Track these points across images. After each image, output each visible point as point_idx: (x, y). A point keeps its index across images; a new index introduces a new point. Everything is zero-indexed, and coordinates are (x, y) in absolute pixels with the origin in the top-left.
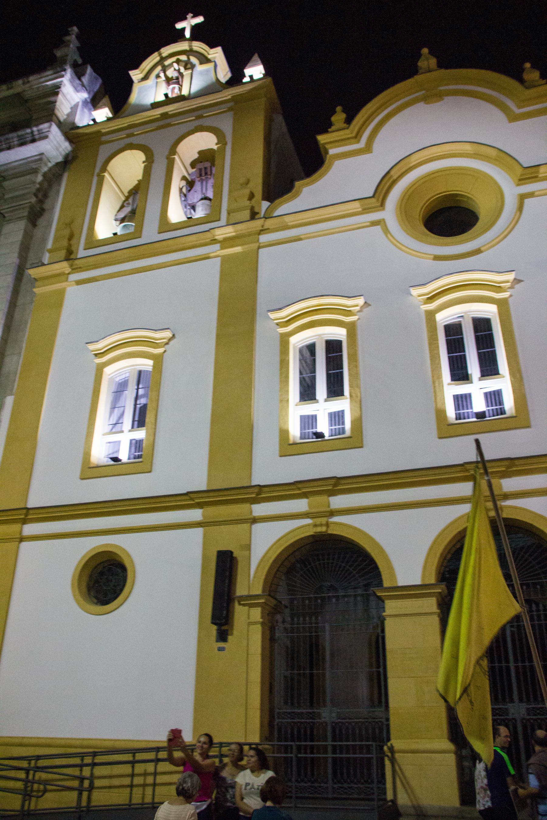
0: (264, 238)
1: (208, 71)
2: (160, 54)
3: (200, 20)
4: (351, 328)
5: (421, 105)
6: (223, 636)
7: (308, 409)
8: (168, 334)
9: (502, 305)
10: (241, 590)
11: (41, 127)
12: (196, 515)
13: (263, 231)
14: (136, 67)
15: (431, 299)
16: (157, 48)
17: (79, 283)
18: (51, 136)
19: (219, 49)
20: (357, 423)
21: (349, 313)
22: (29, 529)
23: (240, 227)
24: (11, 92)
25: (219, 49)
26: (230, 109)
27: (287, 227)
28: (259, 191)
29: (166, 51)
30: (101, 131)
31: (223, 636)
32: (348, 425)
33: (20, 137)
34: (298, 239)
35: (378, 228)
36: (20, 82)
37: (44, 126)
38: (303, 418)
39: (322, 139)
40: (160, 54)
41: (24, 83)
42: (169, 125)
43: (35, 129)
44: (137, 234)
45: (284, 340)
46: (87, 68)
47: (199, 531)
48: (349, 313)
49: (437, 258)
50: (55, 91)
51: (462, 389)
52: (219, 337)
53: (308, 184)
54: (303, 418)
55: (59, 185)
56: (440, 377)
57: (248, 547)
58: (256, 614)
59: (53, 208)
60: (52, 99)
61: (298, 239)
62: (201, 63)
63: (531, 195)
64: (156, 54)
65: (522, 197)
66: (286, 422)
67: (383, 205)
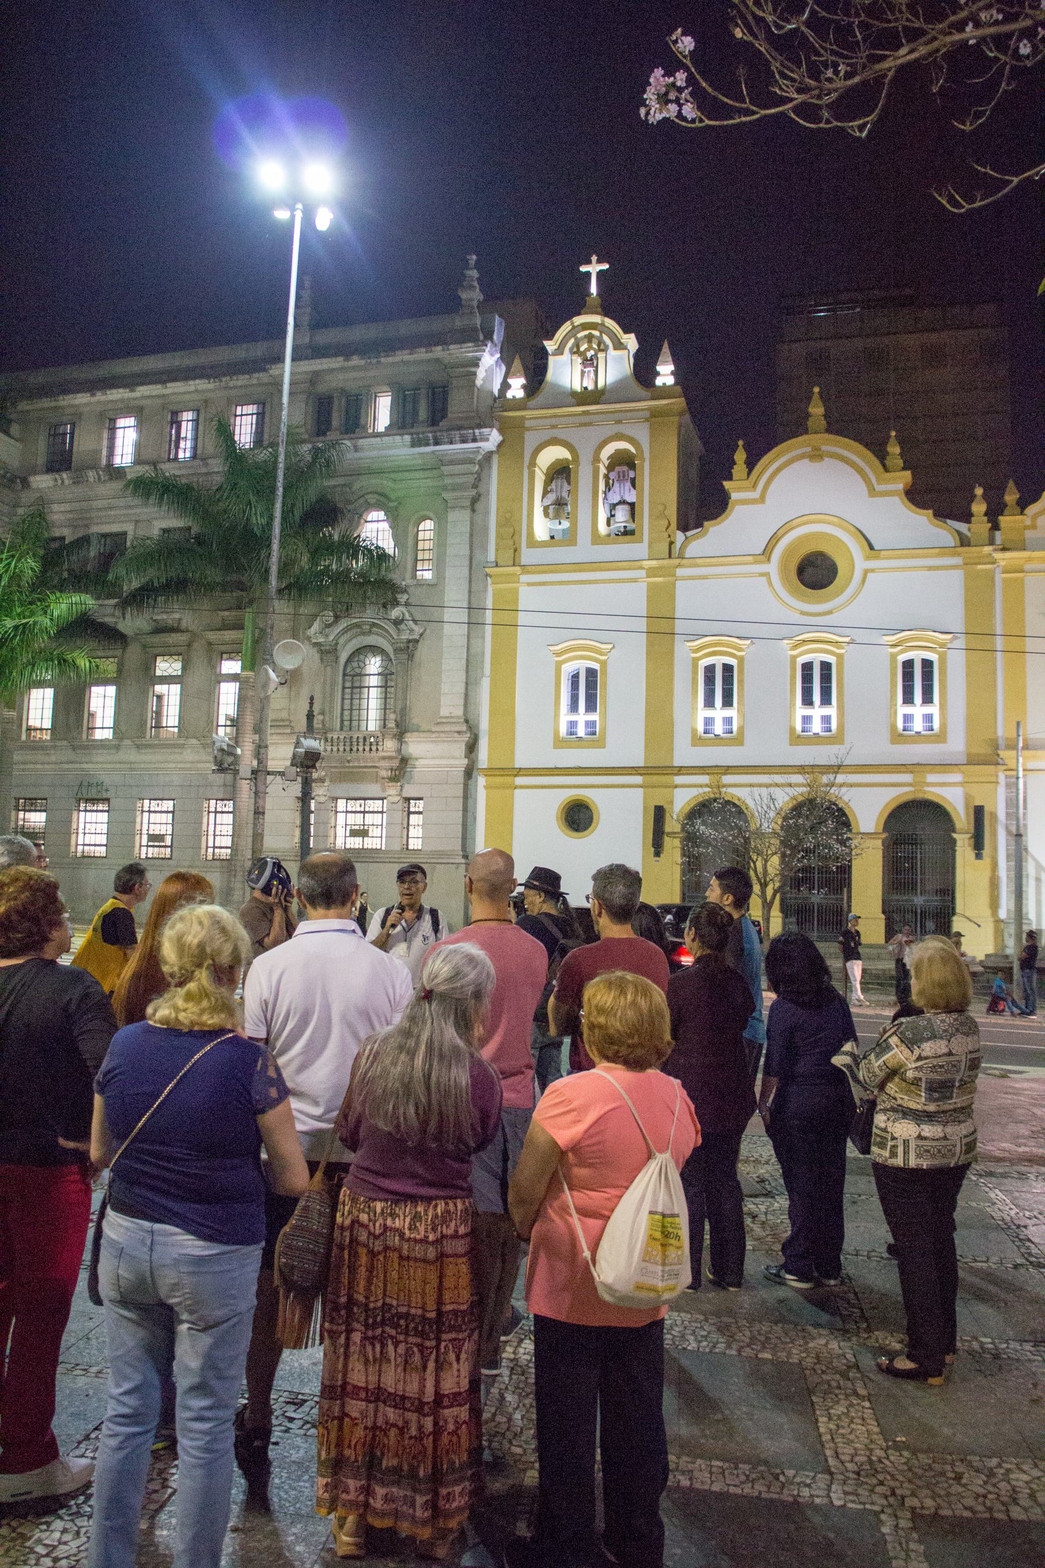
0: (680, 572)
1: (621, 358)
2: (572, 323)
3: (605, 266)
4: (741, 660)
5: (806, 461)
6: (657, 854)
7: (709, 713)
8: (611, 646)
9: (840, 657)
10: (668, 828)
11: (484, 430)
12: (638, 779)
13: (679, 566)
14: (550, 336)
15: (795, 647)
16: (569, 317)
17: (530, 584)
18: (491, 438)
19: (632, 336)
20: (741, 729)
21: (740, 650)
22: (519, 781)
23: (661, 562)
24: (430, 356)
25: (632, 336)
26: (647, 420)
27: (697, 566)
28: (674, 524)
29: (578, 320)
30: (776, 941)
31: (657, 854)
32: (735, 728)
33: (462, 436)
34: (705, 577)
35: (764, 579)
36: (439, 348)
37: (486, 431)
38: (706, 719)
39: (727, 484)
40: (572, 323)
41: (443, 350)
42: (590, 424)
43: (477, 431)
44: (569, 538)
45: (695, 661)
46: (494, 317)
47: (641, 790)
48: (740, 650)
49: (803, 613)
50: (475, 363)
51: (807, 711)
52: (648, 653)
53: (714, 525)
54: (706, 719)
55: (490, 467)
56: (794, 705)
57: (672, 802)
58: (677, 842)
59: (488, 492)
60: (473, 369)
61: (705, 577)
62: (615, 349)
63: (873, 571)
64: (568, 323)
65: (866, 572)
66: (696, 723)
67: (769, 560)
